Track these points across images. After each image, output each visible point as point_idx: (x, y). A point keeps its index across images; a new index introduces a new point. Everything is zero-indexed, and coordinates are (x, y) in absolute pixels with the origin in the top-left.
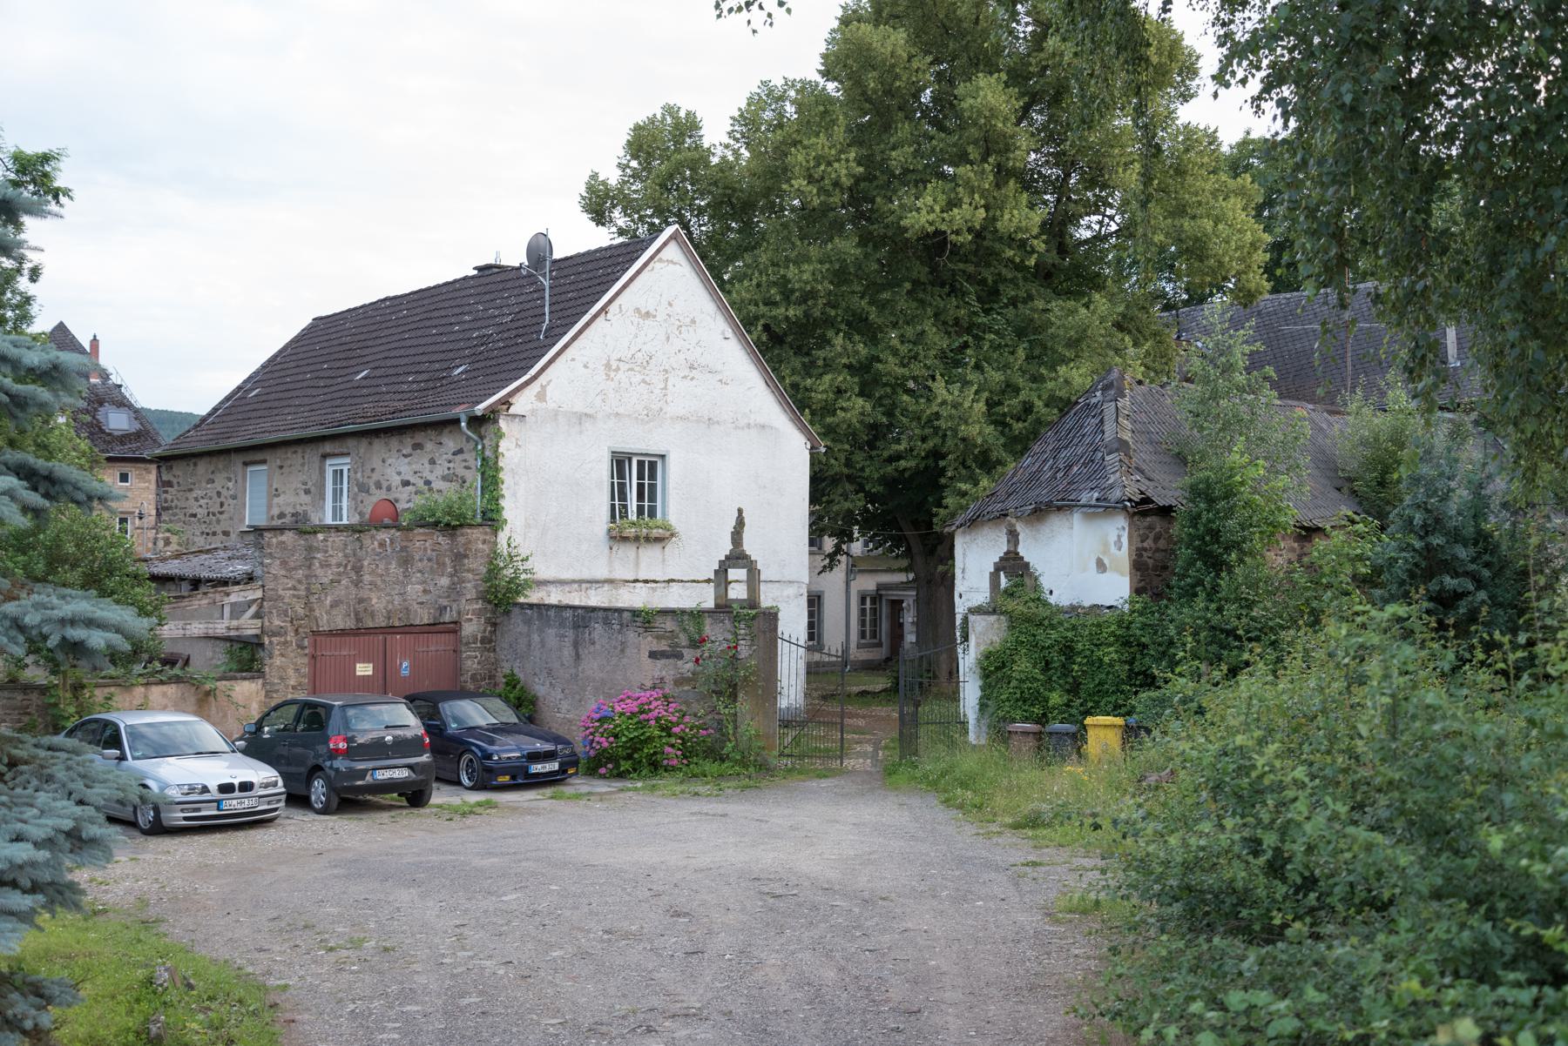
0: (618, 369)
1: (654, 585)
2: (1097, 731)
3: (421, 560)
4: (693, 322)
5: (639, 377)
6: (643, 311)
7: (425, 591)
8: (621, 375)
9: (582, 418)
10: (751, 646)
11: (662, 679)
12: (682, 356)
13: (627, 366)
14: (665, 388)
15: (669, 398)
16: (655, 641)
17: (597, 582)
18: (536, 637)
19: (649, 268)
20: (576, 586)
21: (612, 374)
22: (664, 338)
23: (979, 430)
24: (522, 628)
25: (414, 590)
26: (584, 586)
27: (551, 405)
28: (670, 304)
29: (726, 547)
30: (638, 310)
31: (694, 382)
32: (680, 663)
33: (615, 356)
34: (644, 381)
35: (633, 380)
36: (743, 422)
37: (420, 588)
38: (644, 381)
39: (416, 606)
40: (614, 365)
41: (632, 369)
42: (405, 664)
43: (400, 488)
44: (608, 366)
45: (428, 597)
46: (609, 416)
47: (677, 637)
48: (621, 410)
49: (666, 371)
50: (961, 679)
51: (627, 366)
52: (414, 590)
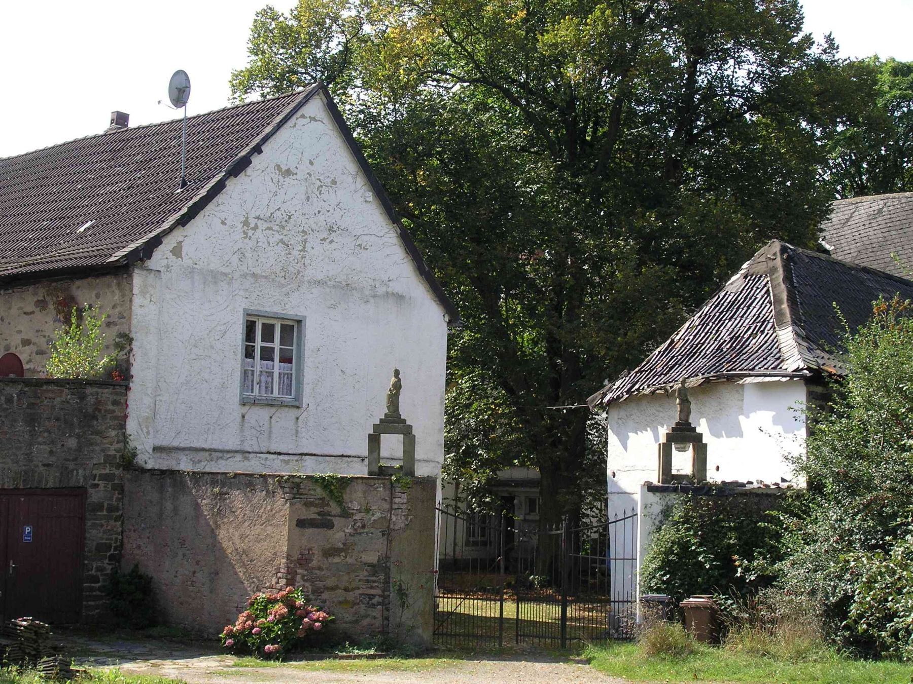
0: (256, 227)
1: (286, 458)
2: (505, 613)
3: (49, 419)
4: (334, 182)
5: (278, 237)
6: (284, 168)
7: (51, 452)
8: (258, 233)
9: (214, 278)
10: (406, 516)
11: (310, 549)
12: (321, 218)
13: (266, 225)
14: (304, 250)
15: (307, 261)
16: (304, 509)
17: (228, 452)
18: (169, 506)
19: (290, 123)
20: (207, 454)
21: (250, 233)
22: (304, 197)
23: (121, 445)
24: (154, 496)
25: (40, 451)
26: (215, 455)
27: (186, 261)
28: (311, 163)
29: (381, 411)
30: (278, 167)
31: (334, 245)
32: (330, 532)
33: (253, 214)
34: (282, 241)
35: (271, 240)
36: (381, 290)
37: (47, 448)
38: (282, 241)
39: (42, 468)
40: (252, 223)
41: (270, 229)
42: (28, 529)
43: (20, 348)
44: (246, 223)
45: (53, 459)
46: (244, 276)
47: (328, 505)
48: (258, 271)
49: (304, 232)
50: (612, 556)
51: (266, 225)
52: (40, 451)
